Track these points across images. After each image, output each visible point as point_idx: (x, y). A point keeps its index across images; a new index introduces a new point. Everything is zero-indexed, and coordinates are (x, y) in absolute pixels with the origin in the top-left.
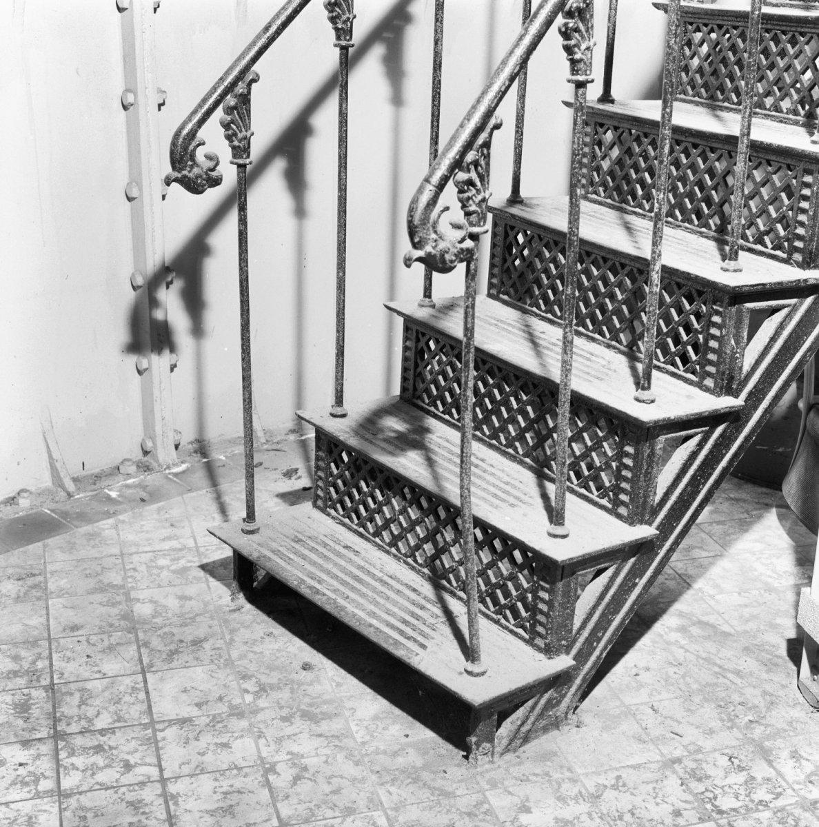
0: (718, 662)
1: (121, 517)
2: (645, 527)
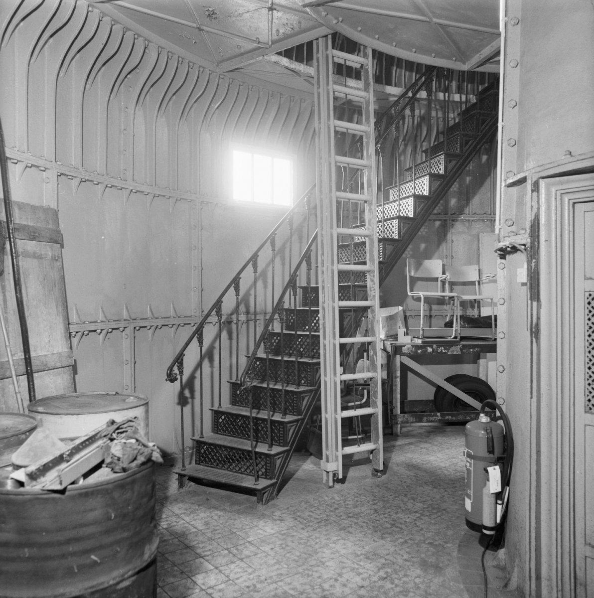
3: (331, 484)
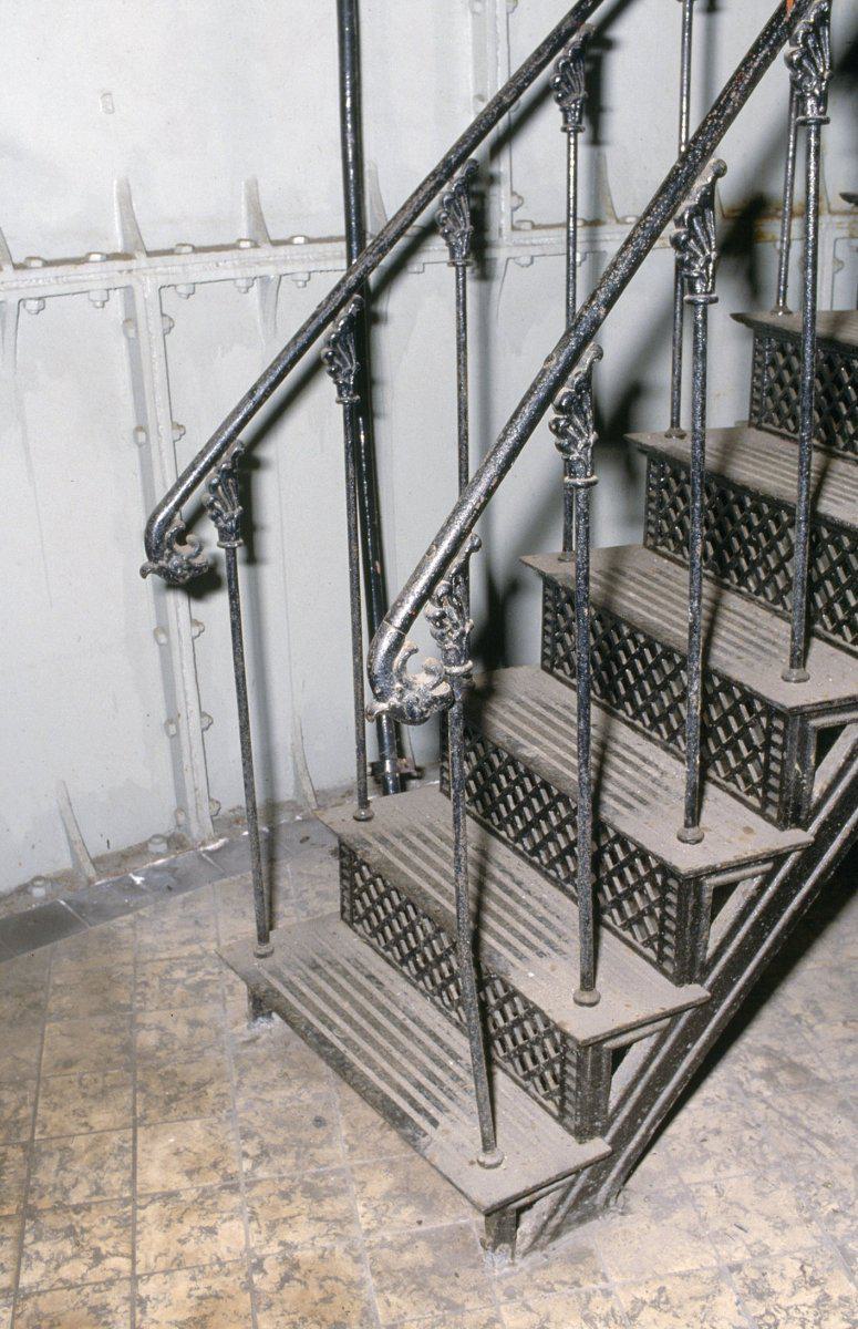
0: (806, 1122)
1: (142, 912)
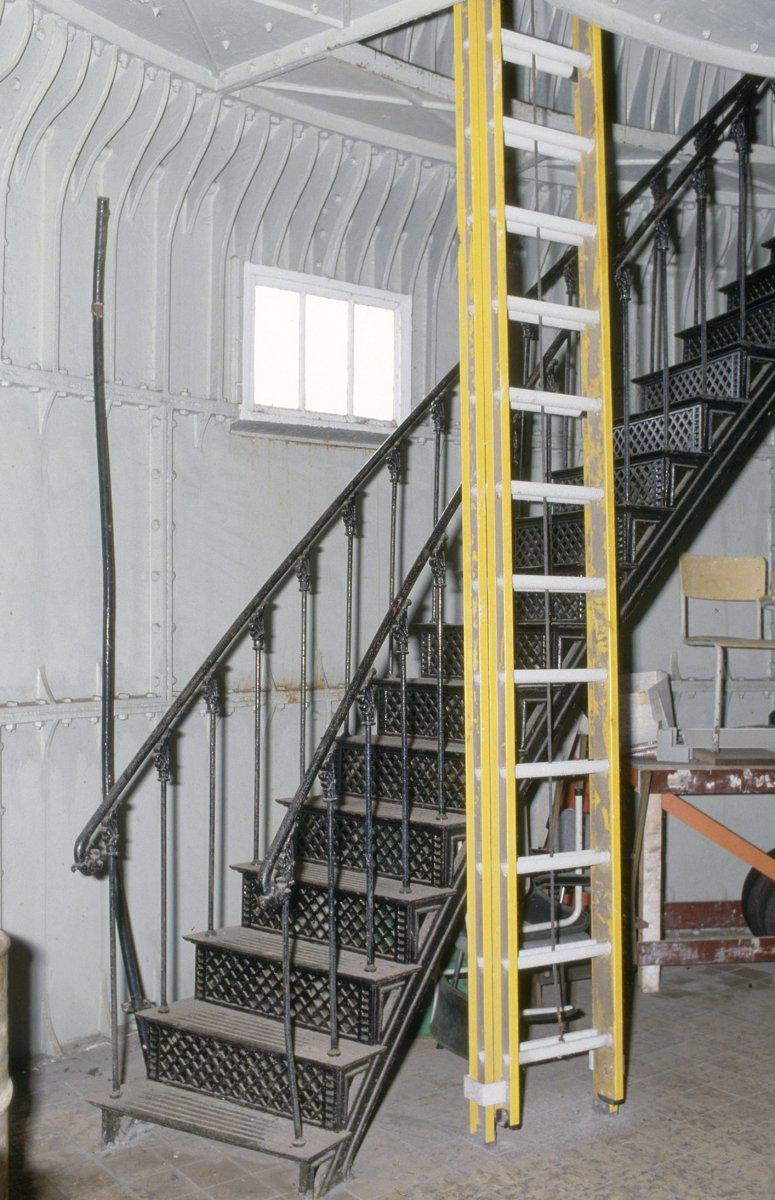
2: (378, 1046)
3: (490, 1137)
